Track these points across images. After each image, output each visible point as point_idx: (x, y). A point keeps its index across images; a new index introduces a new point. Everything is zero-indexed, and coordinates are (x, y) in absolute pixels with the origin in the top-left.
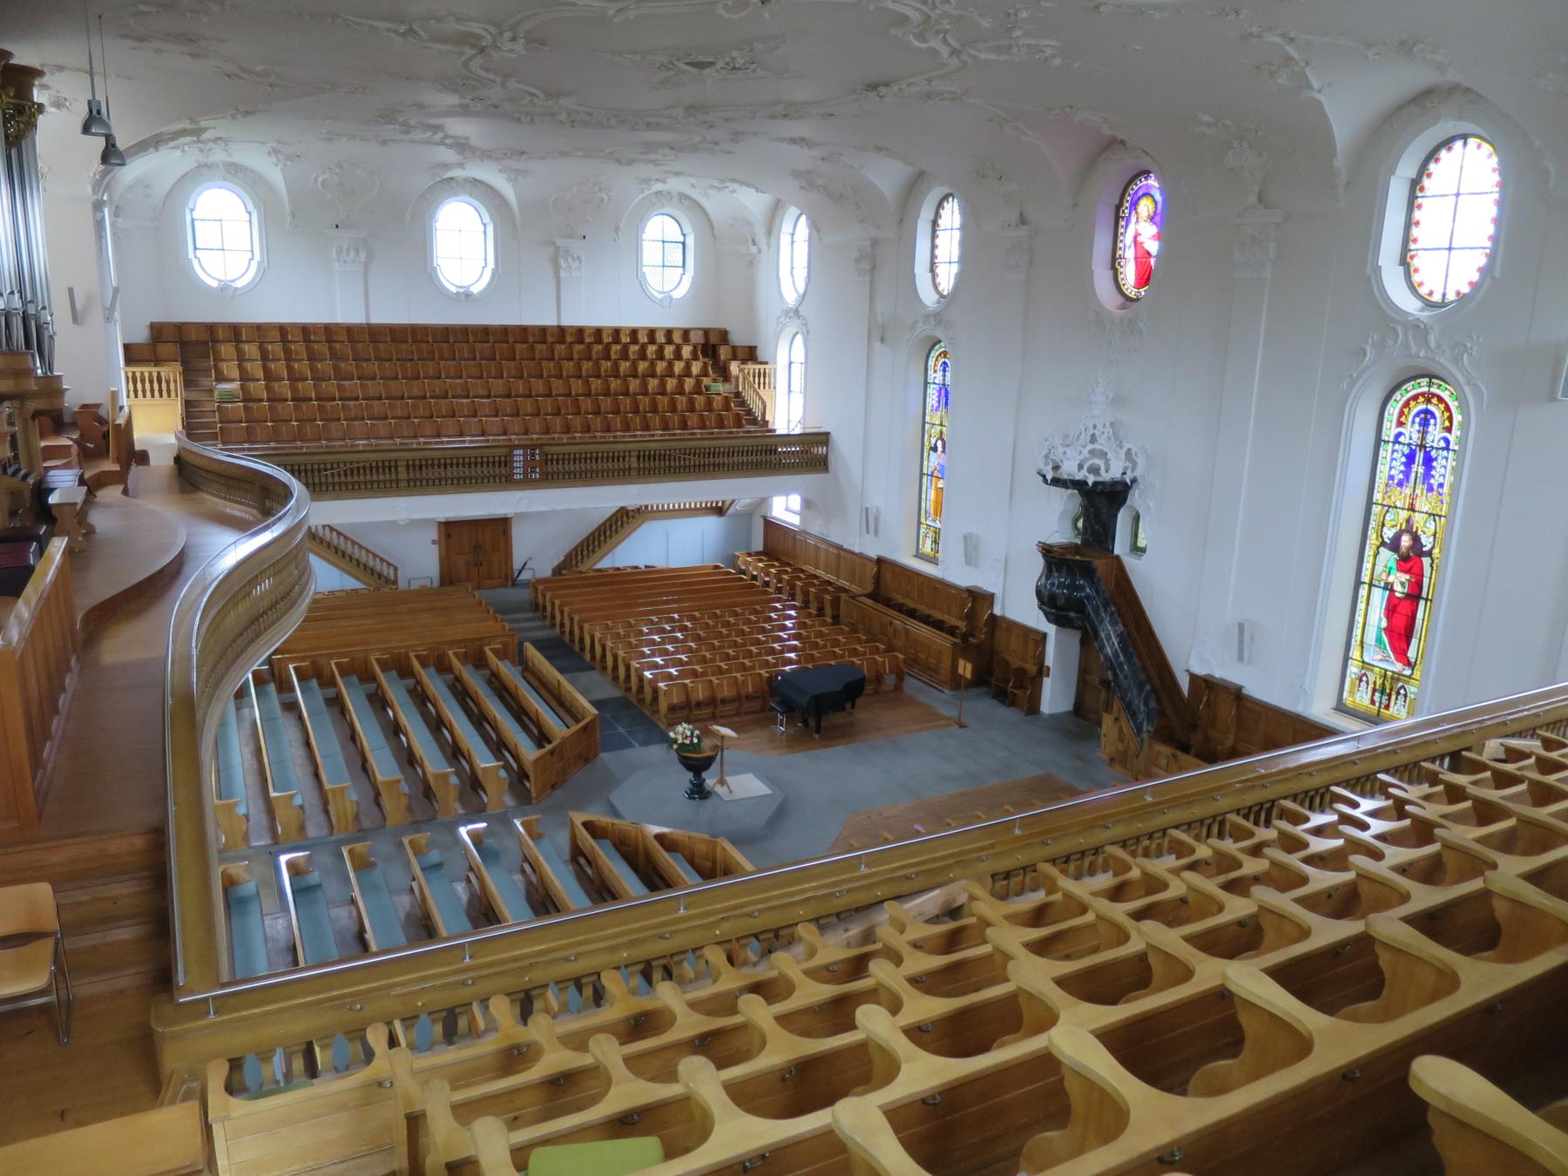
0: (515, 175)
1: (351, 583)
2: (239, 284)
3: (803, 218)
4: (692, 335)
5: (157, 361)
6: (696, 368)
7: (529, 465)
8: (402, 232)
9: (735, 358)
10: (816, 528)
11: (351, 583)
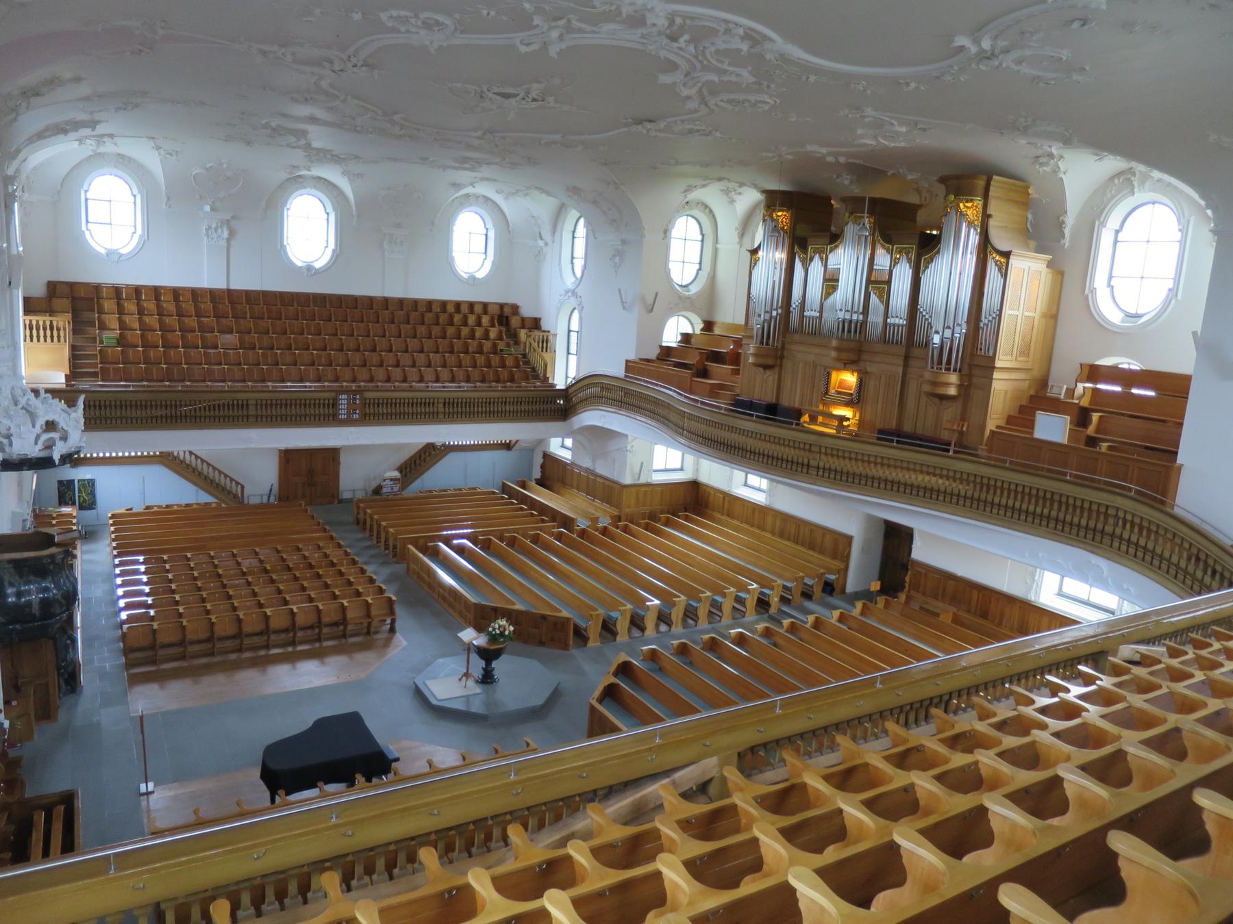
0: (352, 176)
1: (205, 498)
2: (124, 251)
3: (582, 221)
4: (490, 309)
5: (51, 312)
6: (493, 334)
7: (351, 407)
8: (257, 210)
9: (523, 327)
10: (586, 463)
11: (205, 498)
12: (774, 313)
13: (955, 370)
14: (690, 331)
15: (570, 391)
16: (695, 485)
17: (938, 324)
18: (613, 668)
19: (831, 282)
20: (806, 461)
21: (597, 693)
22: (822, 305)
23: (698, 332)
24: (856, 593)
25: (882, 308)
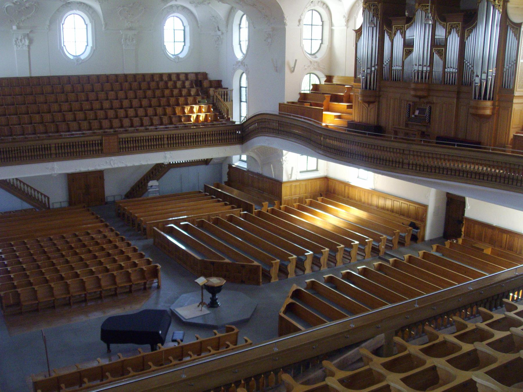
1: (26, 206)
4: (189, 77)
6: (193, 92)
9: (211, 87)
11: (26, 206)
12: (373, 69)
13: (489, 99)
14: (318, 83)
15: (245, 125)
16: (326, 179)
17: (478, 71)
18: (290, 294)
19: (408, 46)
20: (401, 160)
21: (283, 309)
22: (403, 62)
23: (323, 83)
24: (431, 240)
25: (441, 62)
